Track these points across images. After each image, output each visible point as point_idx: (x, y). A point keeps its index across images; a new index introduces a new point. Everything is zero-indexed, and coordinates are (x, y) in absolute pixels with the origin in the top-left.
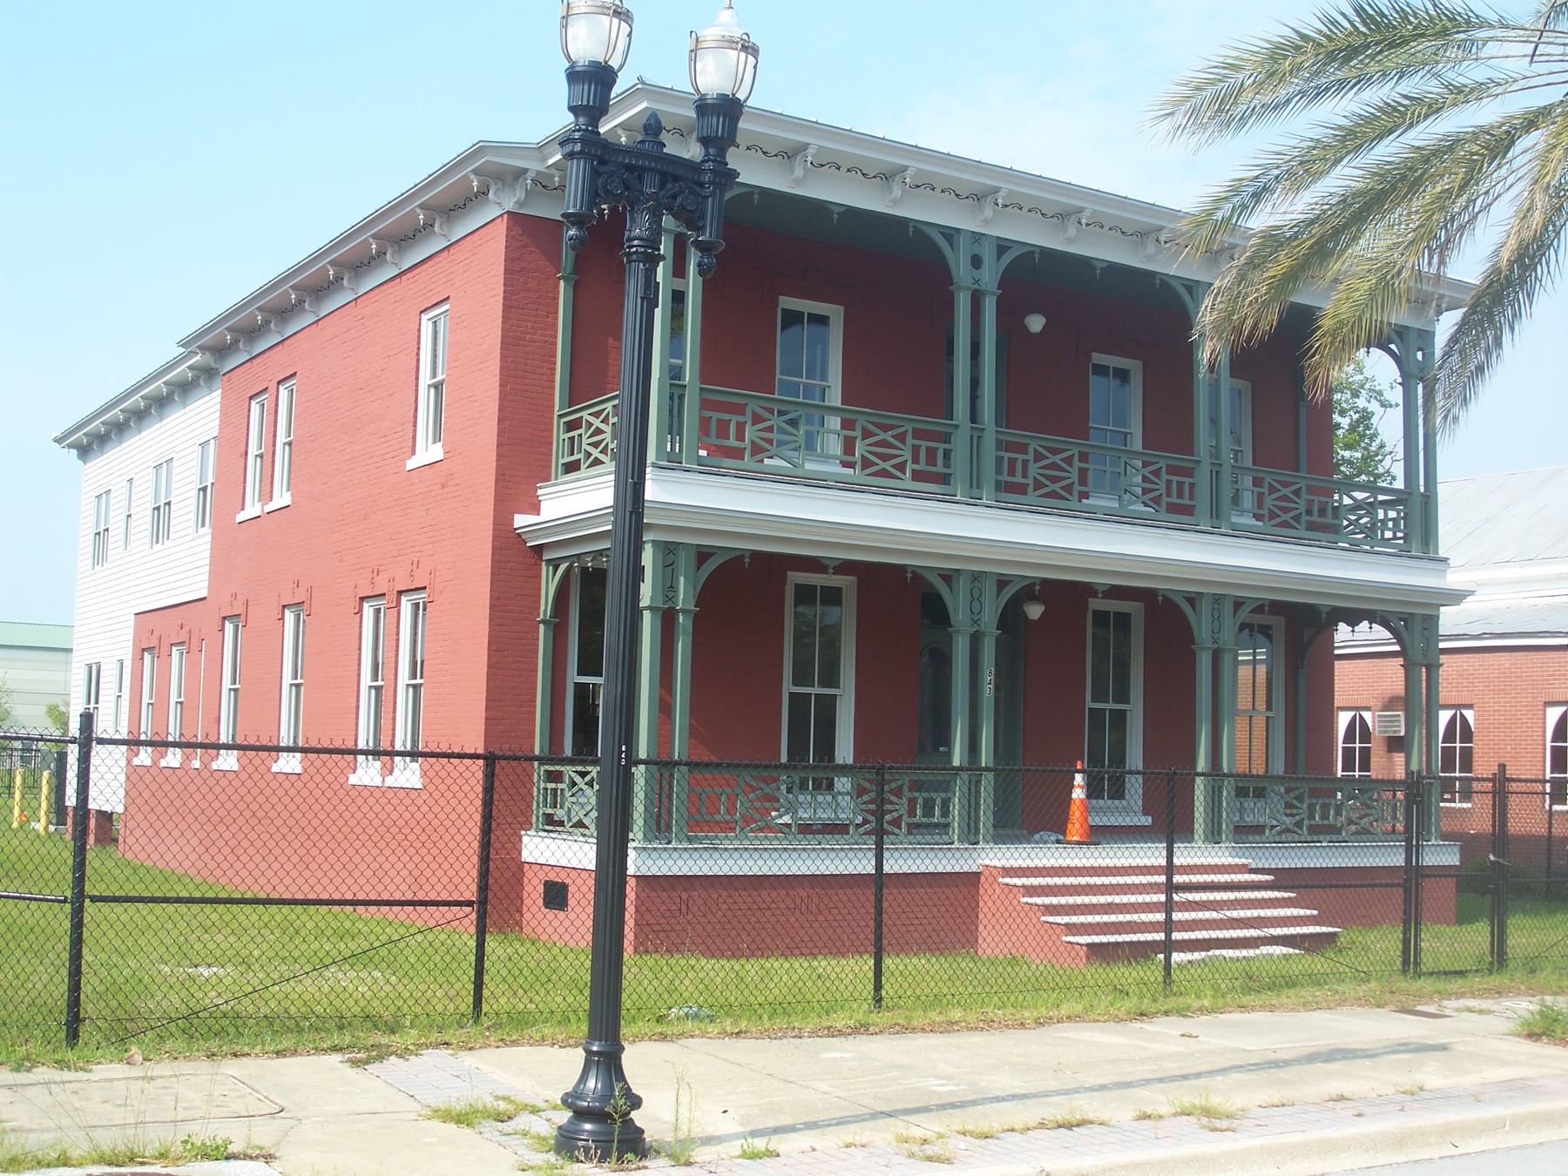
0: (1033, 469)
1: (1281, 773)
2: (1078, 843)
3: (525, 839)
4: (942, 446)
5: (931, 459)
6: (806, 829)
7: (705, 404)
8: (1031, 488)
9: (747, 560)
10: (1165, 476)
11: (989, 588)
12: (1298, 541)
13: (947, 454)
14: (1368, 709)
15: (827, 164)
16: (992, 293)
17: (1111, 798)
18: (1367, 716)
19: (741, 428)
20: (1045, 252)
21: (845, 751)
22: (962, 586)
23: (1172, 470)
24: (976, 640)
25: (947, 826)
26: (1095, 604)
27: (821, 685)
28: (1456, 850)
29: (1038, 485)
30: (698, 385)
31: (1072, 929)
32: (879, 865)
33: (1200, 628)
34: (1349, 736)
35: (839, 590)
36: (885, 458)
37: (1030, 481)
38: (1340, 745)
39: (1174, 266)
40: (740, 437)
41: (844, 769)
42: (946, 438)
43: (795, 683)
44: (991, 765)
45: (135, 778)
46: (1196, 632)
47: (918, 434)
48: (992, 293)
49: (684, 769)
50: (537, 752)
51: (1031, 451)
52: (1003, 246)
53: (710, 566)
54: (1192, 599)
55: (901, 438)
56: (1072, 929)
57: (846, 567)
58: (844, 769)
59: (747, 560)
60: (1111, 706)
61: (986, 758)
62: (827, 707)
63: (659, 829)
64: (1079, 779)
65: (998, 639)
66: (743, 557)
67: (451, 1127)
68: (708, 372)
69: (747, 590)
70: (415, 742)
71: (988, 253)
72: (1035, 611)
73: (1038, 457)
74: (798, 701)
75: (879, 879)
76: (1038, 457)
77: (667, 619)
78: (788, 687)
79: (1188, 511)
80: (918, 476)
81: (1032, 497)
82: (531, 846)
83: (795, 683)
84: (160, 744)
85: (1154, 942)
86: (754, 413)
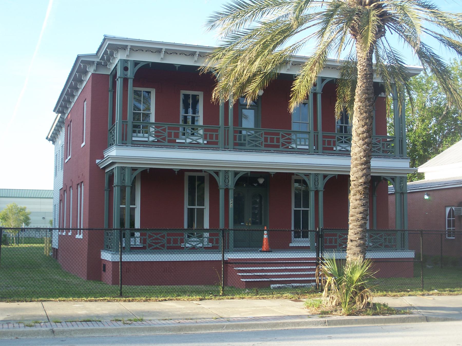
2: (266, 251)
3: (102, 253)
4: (214, 133)
7: (324, 137)
8: (281, 146)
9: (148, 170)
10: (264, 136)
11: (320, 178)
13: (217, 136)
14: (453, 206)
15: (169, 52)
16: (320, 93)
17: (303, 237)
18: (453, 208)
20: (153, 63)
22: (221, 174)
24: (227, 191)
25: (395, 246)
26: (187, 174)
27: (198, 205)
30: (232, 127)
31: (244, 277)
33: (310, 184)
34: (449, 216)
37: (280, 144)
38: (447, 219)
39: (206, 64)
41: (206, 230)
42: (217, 131)
43: (189, 205)
45: (60, 238)
46: (218, 182)
47: (169, 128)
48: (320, 93)
49: (233, 231)
50: (71, 227)
51: (280, 135)
52: (136, 63)
53: (327, 179)
55: (164, 130)
56: (244, 277)
59: (148, 170)
60: (196, 207)
61: (231, 226)
62: (201, 212)
63: (402, 247)
64: (265, 232)
65: (324, 192)
66: (147, 170)
69: (157, 180)
70: (60, 226)
71: (129, 66)
72: (261, 181)
73: (283, 136)
74: (191, 212)
76: (283, 136)
77: (317, 193)
78: (293, 208)
79: (216, 143)
80: (266, 146)
82: (103, 255)
83: (189, 205)
84: (68, 229)
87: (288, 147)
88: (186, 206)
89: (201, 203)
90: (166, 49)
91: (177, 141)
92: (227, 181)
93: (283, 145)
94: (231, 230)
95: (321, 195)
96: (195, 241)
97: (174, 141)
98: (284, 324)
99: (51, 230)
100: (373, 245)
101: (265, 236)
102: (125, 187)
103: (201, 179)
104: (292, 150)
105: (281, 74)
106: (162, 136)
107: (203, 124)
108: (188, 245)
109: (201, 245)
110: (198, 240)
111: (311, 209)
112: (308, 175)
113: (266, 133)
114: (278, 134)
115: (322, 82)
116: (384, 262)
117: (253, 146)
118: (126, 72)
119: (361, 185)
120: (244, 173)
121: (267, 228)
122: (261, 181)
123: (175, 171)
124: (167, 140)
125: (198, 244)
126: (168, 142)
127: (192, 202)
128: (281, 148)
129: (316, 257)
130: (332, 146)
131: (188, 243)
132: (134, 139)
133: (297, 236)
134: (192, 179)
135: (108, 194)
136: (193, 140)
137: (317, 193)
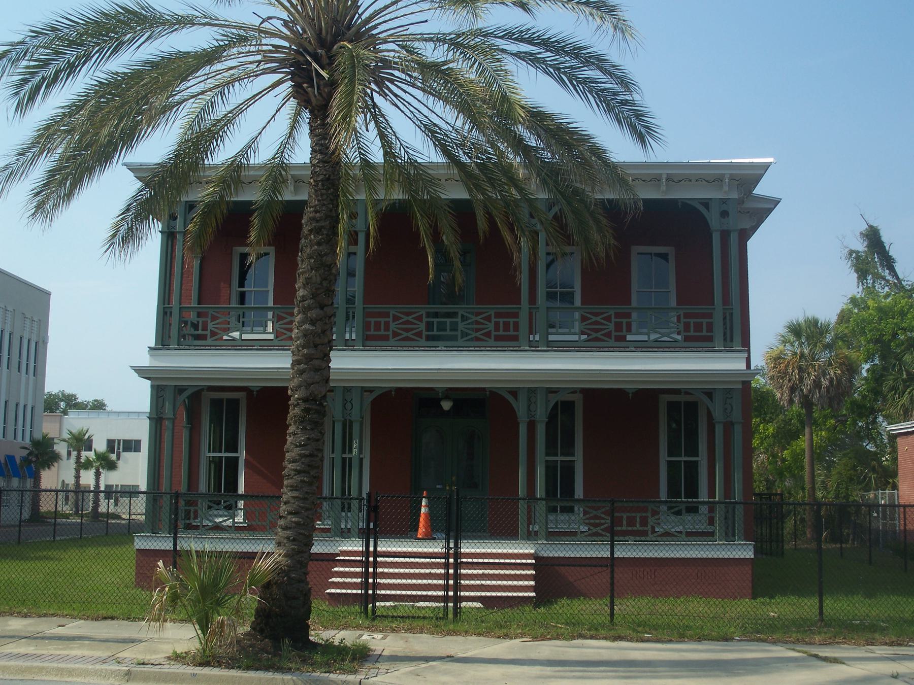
0: (393, 326)
1: (582, 497)
4: (512, 320)
5: (506, 328)
6: (689, 534)
8: (391, 336)
10: (683, 320)
12: (600, 349)
13: (516, 325)
19: (387, 324)
21: (579, 493)
22: (522, 398)
23: (617, 315)
24: (532, 426)
26: (664, 399)
27: (562, 454)
28: (751, 547)
29: (395, 334)
32: (612, 553)
35: (573, 402)
36: (407, 330)
40: (387, 329)
41: (241, 497)
42: (516, 315)
44: (544, 496)
49: (742, 506)
53: (510, 399)
54: (514, 393)
55: (488, 319)
57: (574, 391)
58: (241, 497)
66: (391, 391)
67: (894, 680)
68: (368, 298)
72: (446, 405)
73: (396, 318)
75: (612, 562)
79: (515, 338)
81: (460, 342)
83: (670, 455)
85: (529, 597)
86: (463, 316)
87: (221, 339)
88: (664, 458)
89: (693, 450)
90: (731, 175)
91: (629, 338)
92: (348, 406)
93: (213, 334)
94: (740, 503)
95: (541, 430)
96: (221, 516)
97: (623, 339)
98: (41, 669)
99: (57, 491)
100: (589, 529)
101: (423, 510)
102: (732, 424)
103: (233, 405)
104: (674, 344)
105: (236, 203)
106: (604, 329)
107: (678, 304)
108: (207, 522)
109: (229, 523)
110: (226, 513)
111: (702, 459)
112: (711, 393)
113: (687, 315)
114: (453, 315)
115: (702, 204)
116: (322, 560)
117: (472, 340)
118: (172, 223)
119: (298, 404)
120: (384, 390)
121: (427, 493)
122: (446, 405)
123: (253, 391)
124: (424, 336)
125: (225, 521)
126: (495, 340)
127: (673, 450)
128: (209, 341)
129: (752, 557)
130: (624, 333)
131: (208, 519)
132: (551, 338)
133: (214, 504)
134: (216, 404)
135: (188, 434)
136: (663, 335)
137: (532, 426)
